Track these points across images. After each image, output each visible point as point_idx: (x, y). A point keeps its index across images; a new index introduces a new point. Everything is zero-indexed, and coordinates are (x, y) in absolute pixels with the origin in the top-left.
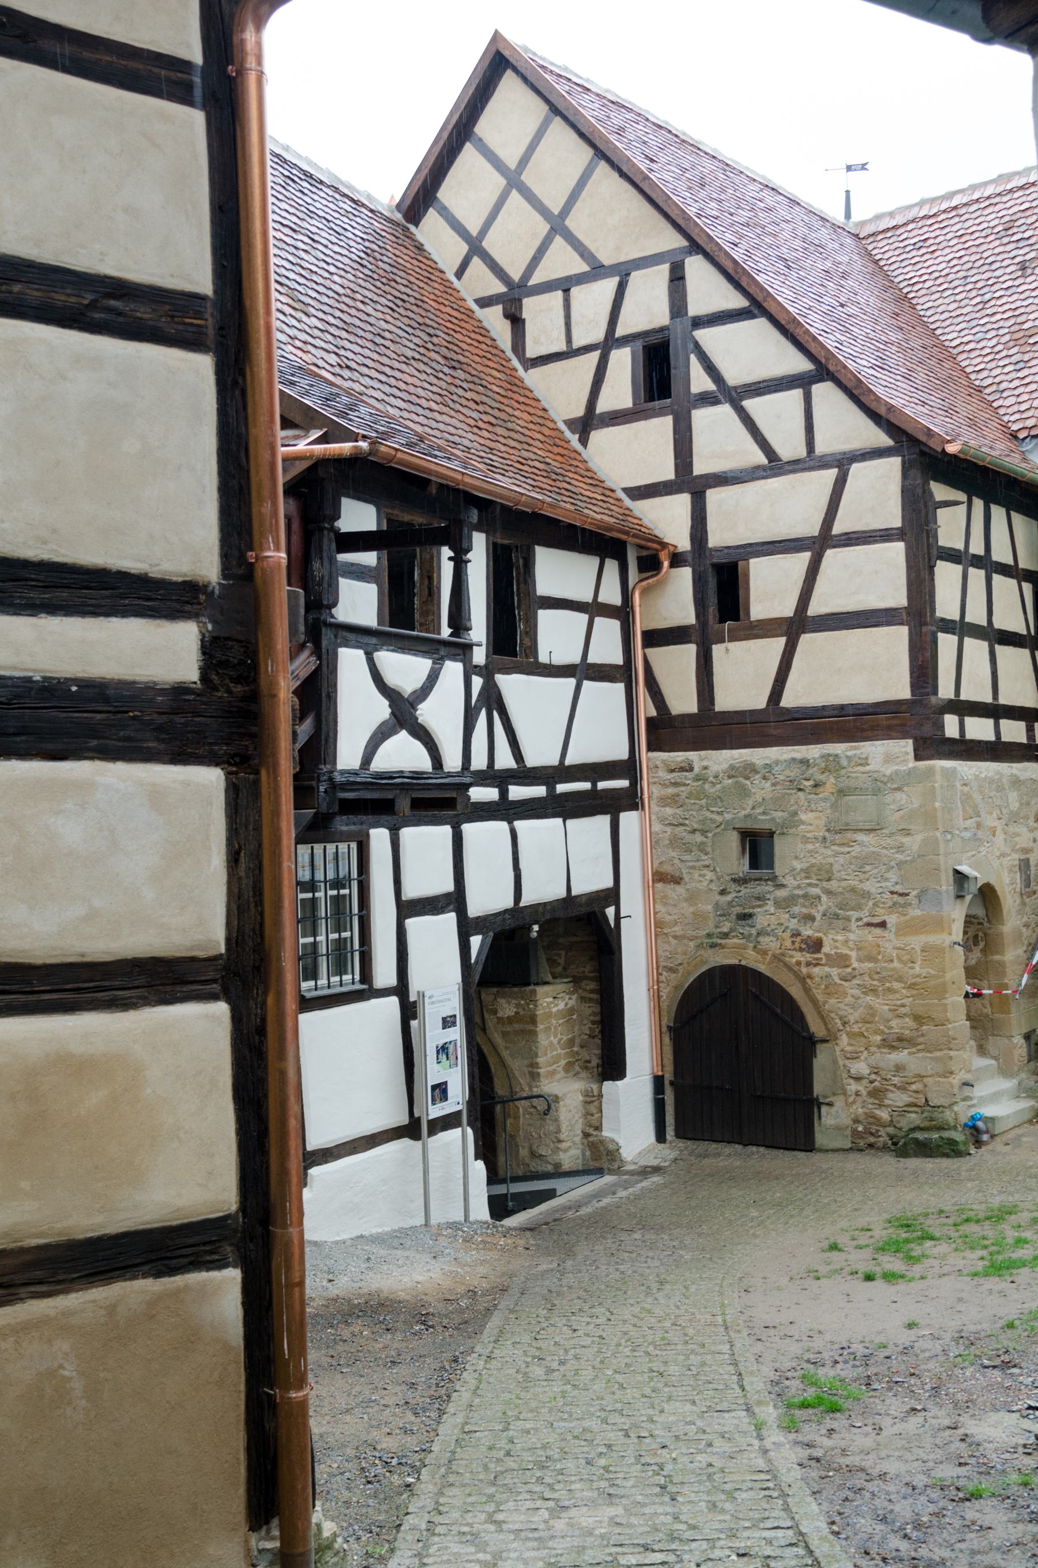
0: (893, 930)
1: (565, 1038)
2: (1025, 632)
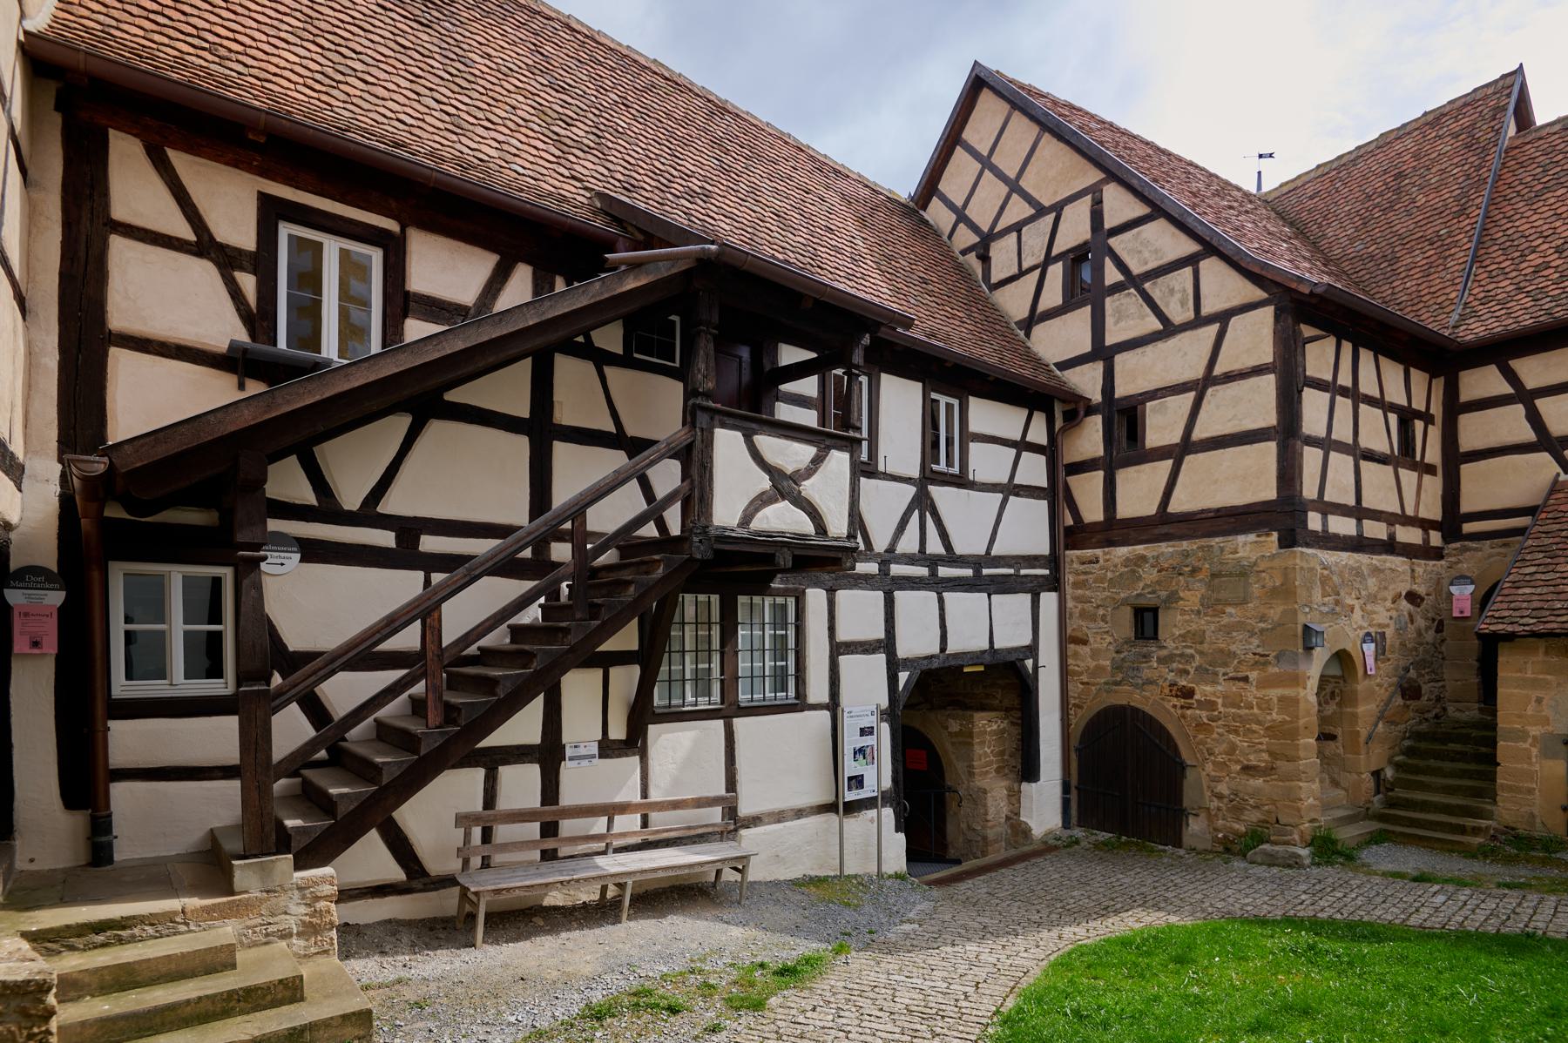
0: (1254, 683)
2: (1389, 452)
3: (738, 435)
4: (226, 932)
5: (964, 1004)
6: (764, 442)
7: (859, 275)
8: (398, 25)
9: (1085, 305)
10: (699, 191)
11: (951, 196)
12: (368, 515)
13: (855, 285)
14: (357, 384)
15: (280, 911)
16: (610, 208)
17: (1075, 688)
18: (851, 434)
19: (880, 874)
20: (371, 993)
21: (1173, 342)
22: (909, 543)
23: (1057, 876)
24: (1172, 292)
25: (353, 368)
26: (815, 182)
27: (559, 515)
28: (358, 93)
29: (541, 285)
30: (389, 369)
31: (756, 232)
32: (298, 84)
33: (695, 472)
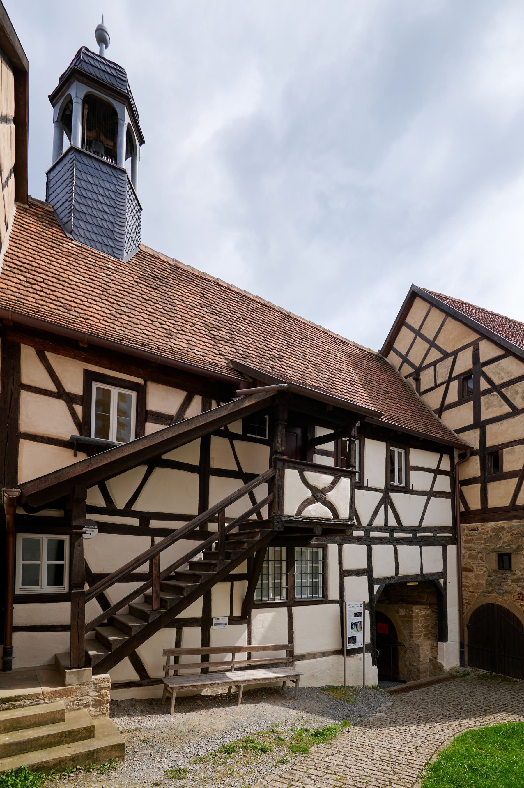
1: (425, 625)
3: (296, 472)
4: (61, 703)
5: (410, 757)
6: (309, 475)
7: (354, 391)
8: (143, 289)
9: (470, 401)
10: (277, 356)
11: (400, 350)
12: (128, 512)
13: (352, 396)
14: (126, 454)
15: (85, 694)
16: (236, 367)
17: (466, 594)
18: (351, 469)
19: (364, 686)
20: (124, 734)
21: (518, 418)
22: (379, 521)
23: (458, 692)
24: (517, 393)
25: (125, 447)
26: (332, 348)
27: (213, 511)
28: (126, 322)
29: (206, 406)
30: (140, 447)
31: (305, 374)
32: (101, 320)
33: (275, 489)
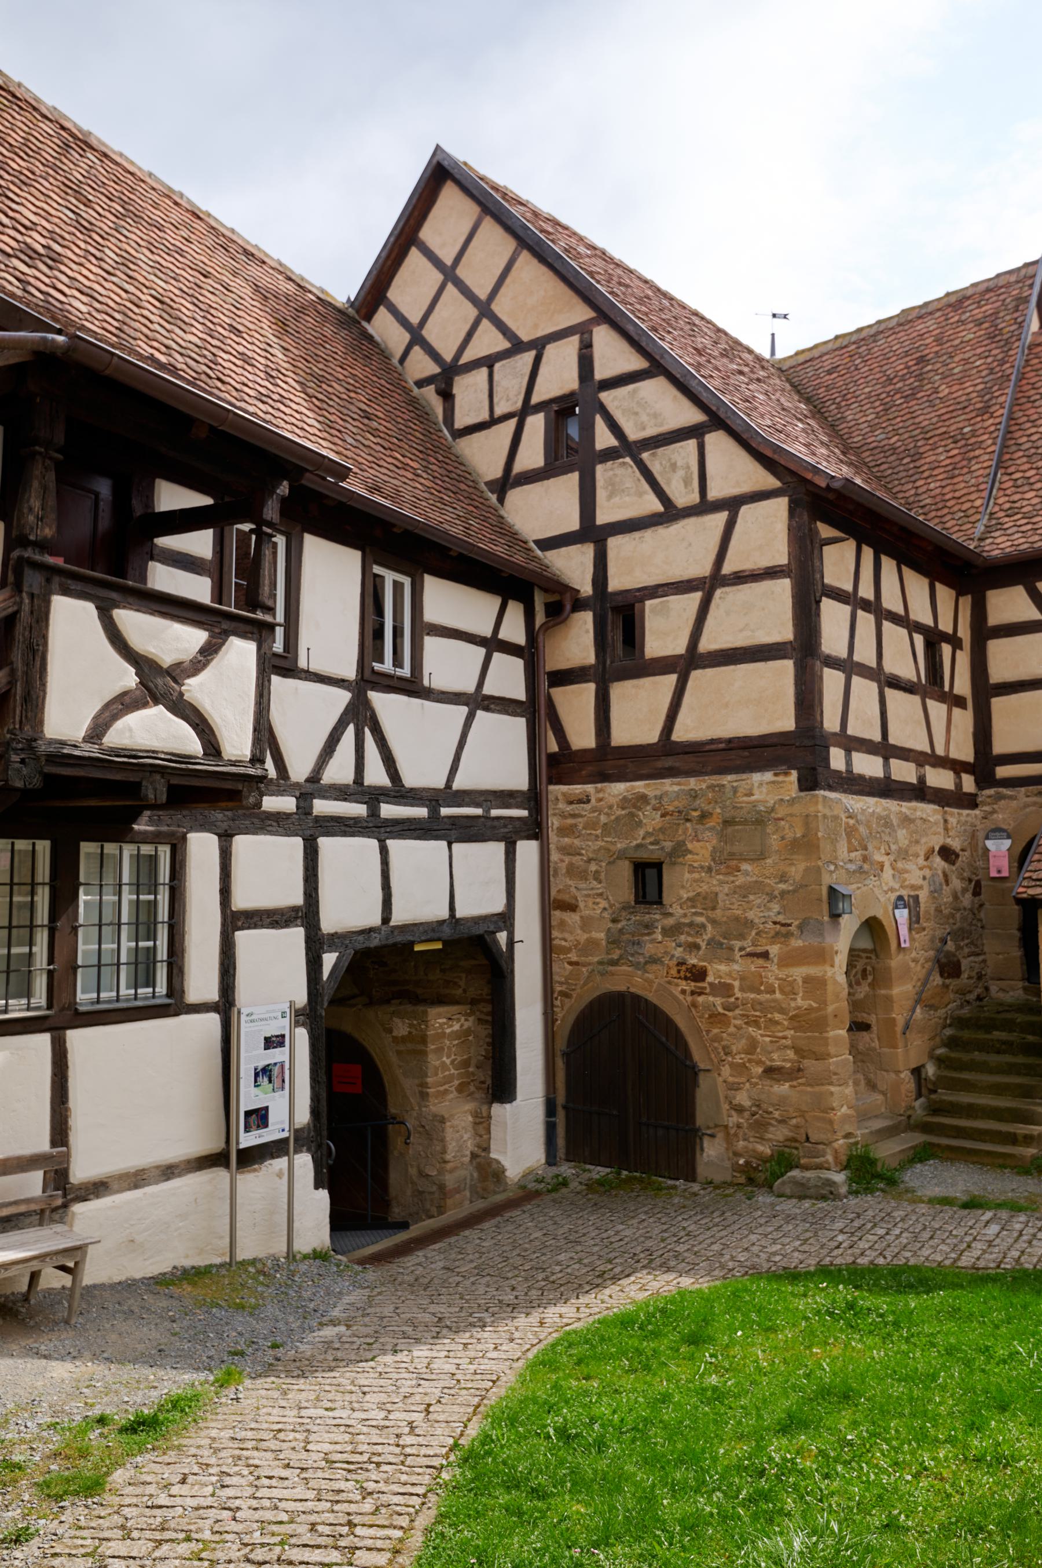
0: (776, 960)
1: (459, 1059)
2: (915, 679)
